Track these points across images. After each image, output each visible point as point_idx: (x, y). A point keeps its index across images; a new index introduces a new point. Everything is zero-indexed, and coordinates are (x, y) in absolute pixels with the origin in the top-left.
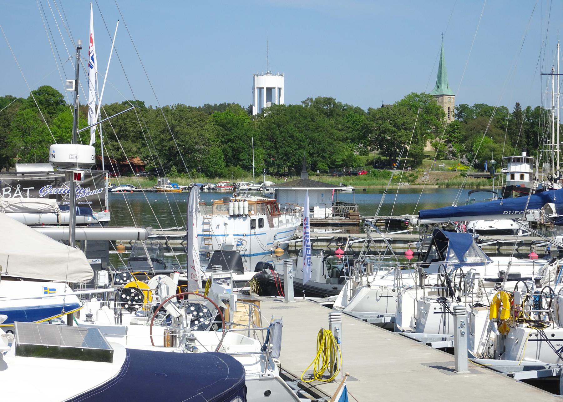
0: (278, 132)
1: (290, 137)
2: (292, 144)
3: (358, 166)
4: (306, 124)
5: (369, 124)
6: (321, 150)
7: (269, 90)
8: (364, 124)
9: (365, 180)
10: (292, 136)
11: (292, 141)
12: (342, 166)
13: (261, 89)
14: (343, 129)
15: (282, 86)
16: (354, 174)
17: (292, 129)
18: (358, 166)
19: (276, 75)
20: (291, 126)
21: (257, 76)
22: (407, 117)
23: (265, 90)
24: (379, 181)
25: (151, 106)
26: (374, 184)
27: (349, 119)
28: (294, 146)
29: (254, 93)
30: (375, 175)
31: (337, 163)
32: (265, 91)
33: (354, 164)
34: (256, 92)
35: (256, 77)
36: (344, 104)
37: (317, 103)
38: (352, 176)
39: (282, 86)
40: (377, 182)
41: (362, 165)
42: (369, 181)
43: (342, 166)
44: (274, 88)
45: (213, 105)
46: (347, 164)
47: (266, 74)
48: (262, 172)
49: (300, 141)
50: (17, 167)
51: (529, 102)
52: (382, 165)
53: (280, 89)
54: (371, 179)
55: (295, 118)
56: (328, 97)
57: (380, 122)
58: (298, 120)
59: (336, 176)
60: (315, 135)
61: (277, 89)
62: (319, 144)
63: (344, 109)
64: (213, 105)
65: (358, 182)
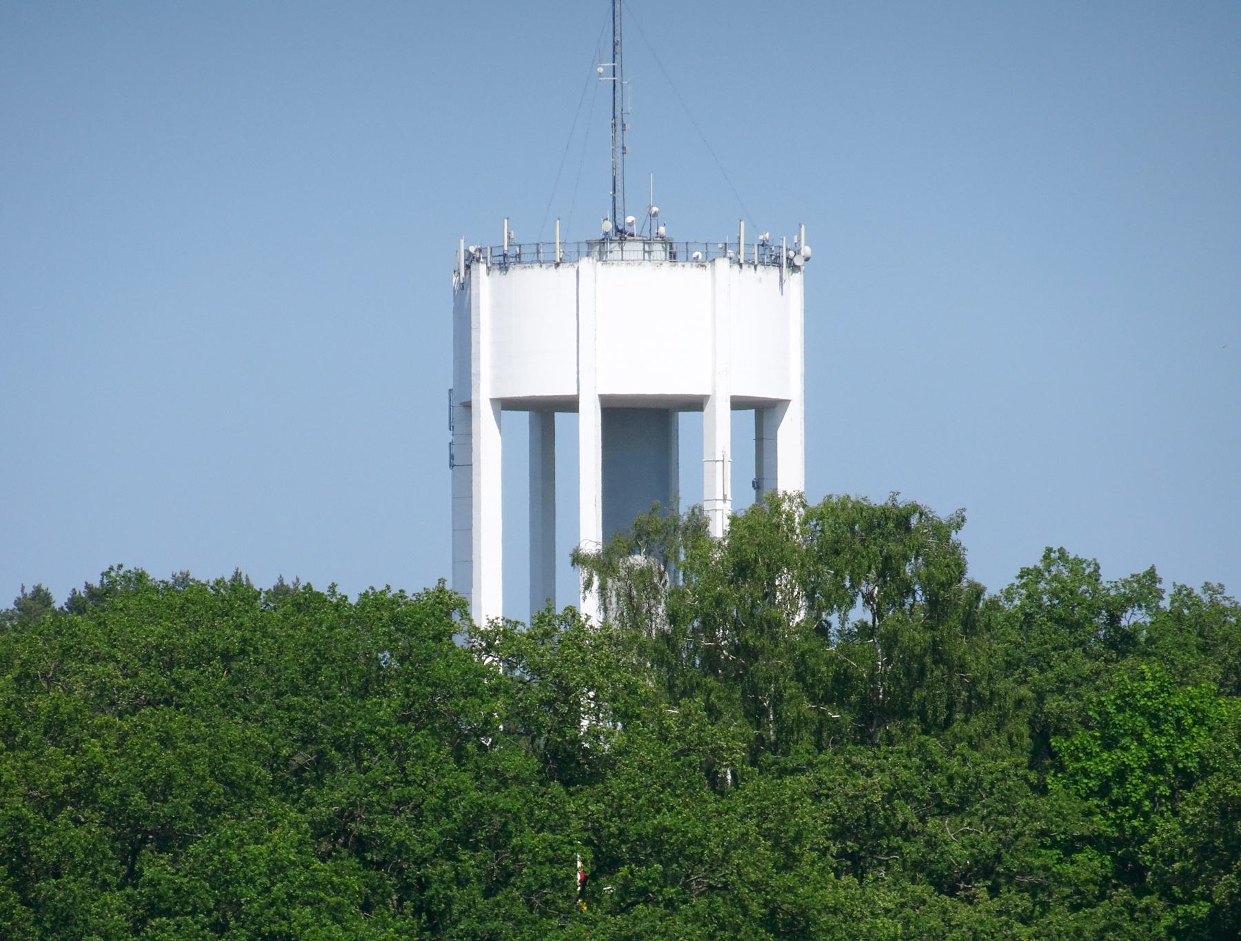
4: (478, 815)
13: (545, 414)
15: (784, 379)
17: (277, 869)
19: (708, 260)
21: (503, 264)
29: (461, 461)
32: (586, 438)
34: (491, 444)
35: (485, 282)
39: (784, 379)
44: (696, 404)
47: (599, 247)
51: (984, 584)
53: (762, 413)
55: (354, 748)
56: (878, 499)
58: (381, 767)
61: (720, 419)
63: (1123, 642)
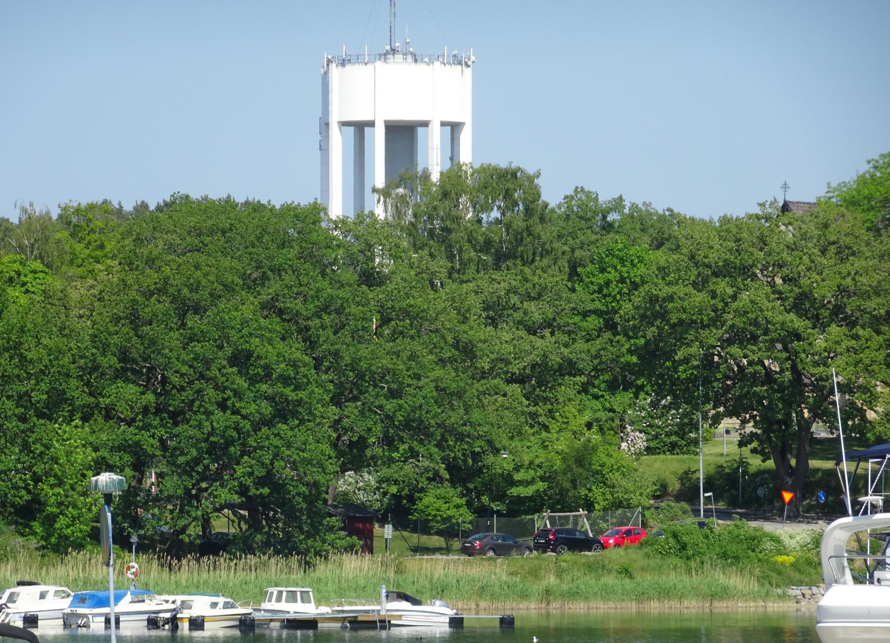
0: (174, 339)
1: (234, 360)
2: (238, 394)
3: (618, 504)
5: (671, 298)
6: (407, 425)
7: (402, 135)
8: (653, 300)
9: (626, 572)
10: (241, 360)
11: (241, 383)
12: (535, 504)
13: (361, 128)
14: (549, 324)
16: (581, 544)
18: (618, 504)
19: (431, 62)
20: (246, 308)
21: (343, 63)
22: (858, 264)
23: (380, 133)
24: (696, 580)
25: (48, 213)
26: (665, 593)
27: (612, 275)
28: (253, 408)
29: (324, 148)
30: (684, 547)
31: (514, 491)
32: (378, 139)
33: (599, 495)
35: (335, 71)
36: (605, 197)
37: (445, 195)
38: (567, 556)
39: (462, 113)
40: (674, 578)
41: (635, 499)
42: (646, 580)
43: (535, 504)
44: (425, 124)
45: (128, 207)
46: (563, 492)
47: (384, 56)
48: (95, 536)
49: (285, 380)
50: (810, 461)
52: (739, 493)
53: (454, 128)
54: (659, 569)
55: (278, 271)
57: (723, 286)
58: (289, 278)
59: (482, 551)
60: (376, 354)
62: (394, 394)
63: (608, 227)
64: (128, 207)
65: (588, 581)
